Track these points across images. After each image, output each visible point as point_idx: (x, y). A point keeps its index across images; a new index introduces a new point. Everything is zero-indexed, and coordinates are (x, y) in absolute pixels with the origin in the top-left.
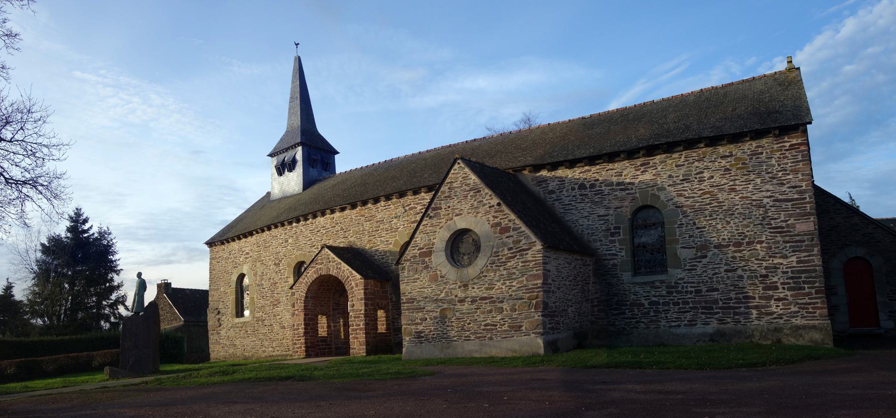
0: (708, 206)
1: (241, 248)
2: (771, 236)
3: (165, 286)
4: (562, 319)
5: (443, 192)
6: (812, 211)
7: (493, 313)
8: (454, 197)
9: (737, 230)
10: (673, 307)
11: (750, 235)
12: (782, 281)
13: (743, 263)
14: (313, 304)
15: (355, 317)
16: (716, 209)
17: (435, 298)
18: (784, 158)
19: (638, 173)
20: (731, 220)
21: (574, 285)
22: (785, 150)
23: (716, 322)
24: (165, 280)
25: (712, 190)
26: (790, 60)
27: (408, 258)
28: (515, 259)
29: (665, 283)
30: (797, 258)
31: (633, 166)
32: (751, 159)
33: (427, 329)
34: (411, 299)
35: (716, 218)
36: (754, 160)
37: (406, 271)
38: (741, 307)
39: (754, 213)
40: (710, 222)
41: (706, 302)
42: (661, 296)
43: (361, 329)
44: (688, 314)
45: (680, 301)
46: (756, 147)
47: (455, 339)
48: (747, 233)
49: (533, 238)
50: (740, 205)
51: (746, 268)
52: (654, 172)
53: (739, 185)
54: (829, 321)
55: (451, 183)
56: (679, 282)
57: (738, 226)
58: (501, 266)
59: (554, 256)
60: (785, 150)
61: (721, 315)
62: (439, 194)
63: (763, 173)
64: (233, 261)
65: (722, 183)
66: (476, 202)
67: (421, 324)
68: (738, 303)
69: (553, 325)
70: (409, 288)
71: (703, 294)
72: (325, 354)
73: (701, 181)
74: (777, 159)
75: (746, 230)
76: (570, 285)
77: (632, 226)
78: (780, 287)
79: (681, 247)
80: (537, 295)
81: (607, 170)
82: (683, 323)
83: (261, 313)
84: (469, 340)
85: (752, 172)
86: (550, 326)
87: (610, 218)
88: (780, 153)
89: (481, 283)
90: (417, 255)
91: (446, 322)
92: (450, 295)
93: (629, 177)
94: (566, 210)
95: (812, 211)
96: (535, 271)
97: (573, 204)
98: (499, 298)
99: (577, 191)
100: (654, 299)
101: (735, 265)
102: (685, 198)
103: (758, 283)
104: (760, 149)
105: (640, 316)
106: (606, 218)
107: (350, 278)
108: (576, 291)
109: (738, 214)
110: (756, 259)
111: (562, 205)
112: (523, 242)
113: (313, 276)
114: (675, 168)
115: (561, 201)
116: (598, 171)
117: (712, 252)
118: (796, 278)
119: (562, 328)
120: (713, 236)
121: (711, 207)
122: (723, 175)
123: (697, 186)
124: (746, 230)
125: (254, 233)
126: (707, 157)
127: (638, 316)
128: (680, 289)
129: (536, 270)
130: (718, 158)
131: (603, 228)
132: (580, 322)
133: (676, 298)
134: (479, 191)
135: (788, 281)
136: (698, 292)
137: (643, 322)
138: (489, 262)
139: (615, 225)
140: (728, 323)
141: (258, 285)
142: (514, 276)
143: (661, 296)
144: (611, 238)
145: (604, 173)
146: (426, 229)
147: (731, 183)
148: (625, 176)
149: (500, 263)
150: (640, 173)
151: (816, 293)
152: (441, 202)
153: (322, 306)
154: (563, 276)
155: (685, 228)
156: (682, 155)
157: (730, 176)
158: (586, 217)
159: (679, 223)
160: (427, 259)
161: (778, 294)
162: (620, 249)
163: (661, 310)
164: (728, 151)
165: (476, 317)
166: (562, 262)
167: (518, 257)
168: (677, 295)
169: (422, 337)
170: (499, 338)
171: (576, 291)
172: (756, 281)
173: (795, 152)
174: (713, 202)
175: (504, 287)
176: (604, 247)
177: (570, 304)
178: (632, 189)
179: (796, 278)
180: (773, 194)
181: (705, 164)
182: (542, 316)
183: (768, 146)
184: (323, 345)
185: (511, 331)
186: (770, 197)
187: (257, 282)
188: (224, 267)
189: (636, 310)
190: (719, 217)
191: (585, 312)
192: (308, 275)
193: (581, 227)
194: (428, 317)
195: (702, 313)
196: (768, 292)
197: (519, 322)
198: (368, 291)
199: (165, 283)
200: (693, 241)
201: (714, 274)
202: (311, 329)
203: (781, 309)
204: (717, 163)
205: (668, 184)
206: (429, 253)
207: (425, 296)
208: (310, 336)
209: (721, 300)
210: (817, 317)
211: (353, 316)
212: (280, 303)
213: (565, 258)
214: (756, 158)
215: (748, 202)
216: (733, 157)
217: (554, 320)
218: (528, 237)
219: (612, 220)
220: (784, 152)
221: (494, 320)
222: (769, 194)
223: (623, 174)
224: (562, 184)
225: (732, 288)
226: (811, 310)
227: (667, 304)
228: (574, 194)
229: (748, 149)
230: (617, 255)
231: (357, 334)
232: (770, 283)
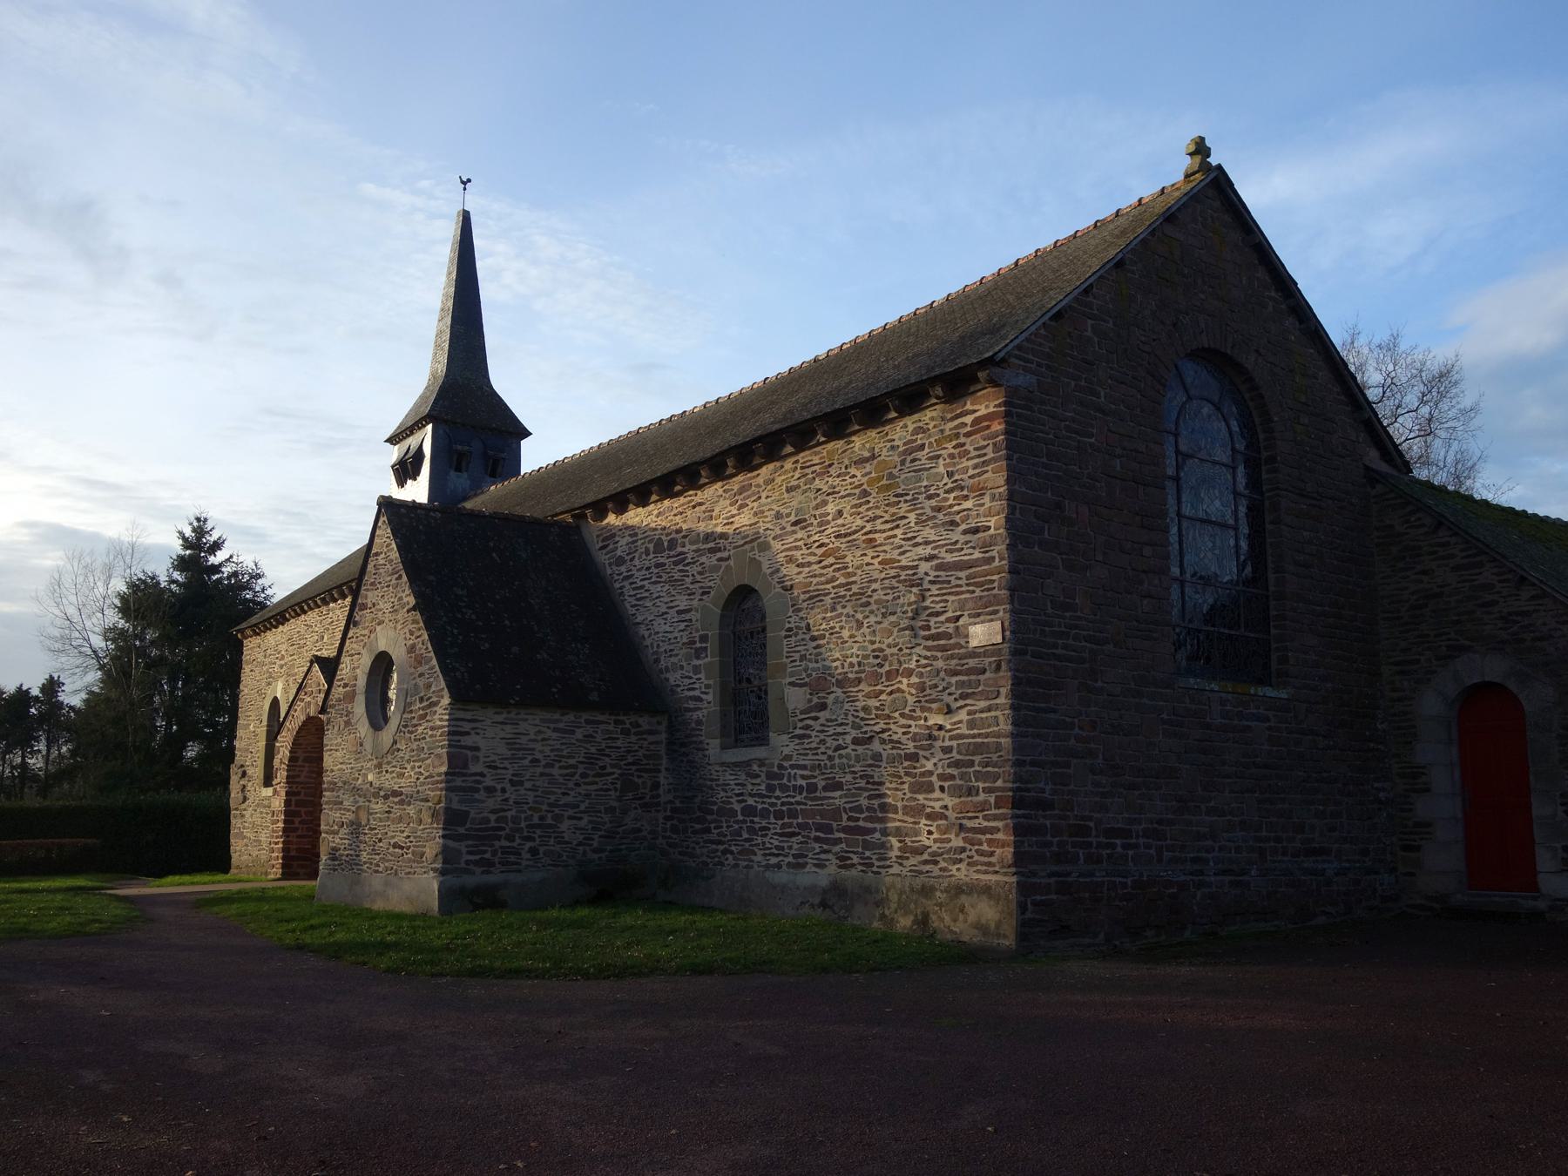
78: (937, 784)
88: (954, 443)
220: (962, 440)
222: (928, 550)
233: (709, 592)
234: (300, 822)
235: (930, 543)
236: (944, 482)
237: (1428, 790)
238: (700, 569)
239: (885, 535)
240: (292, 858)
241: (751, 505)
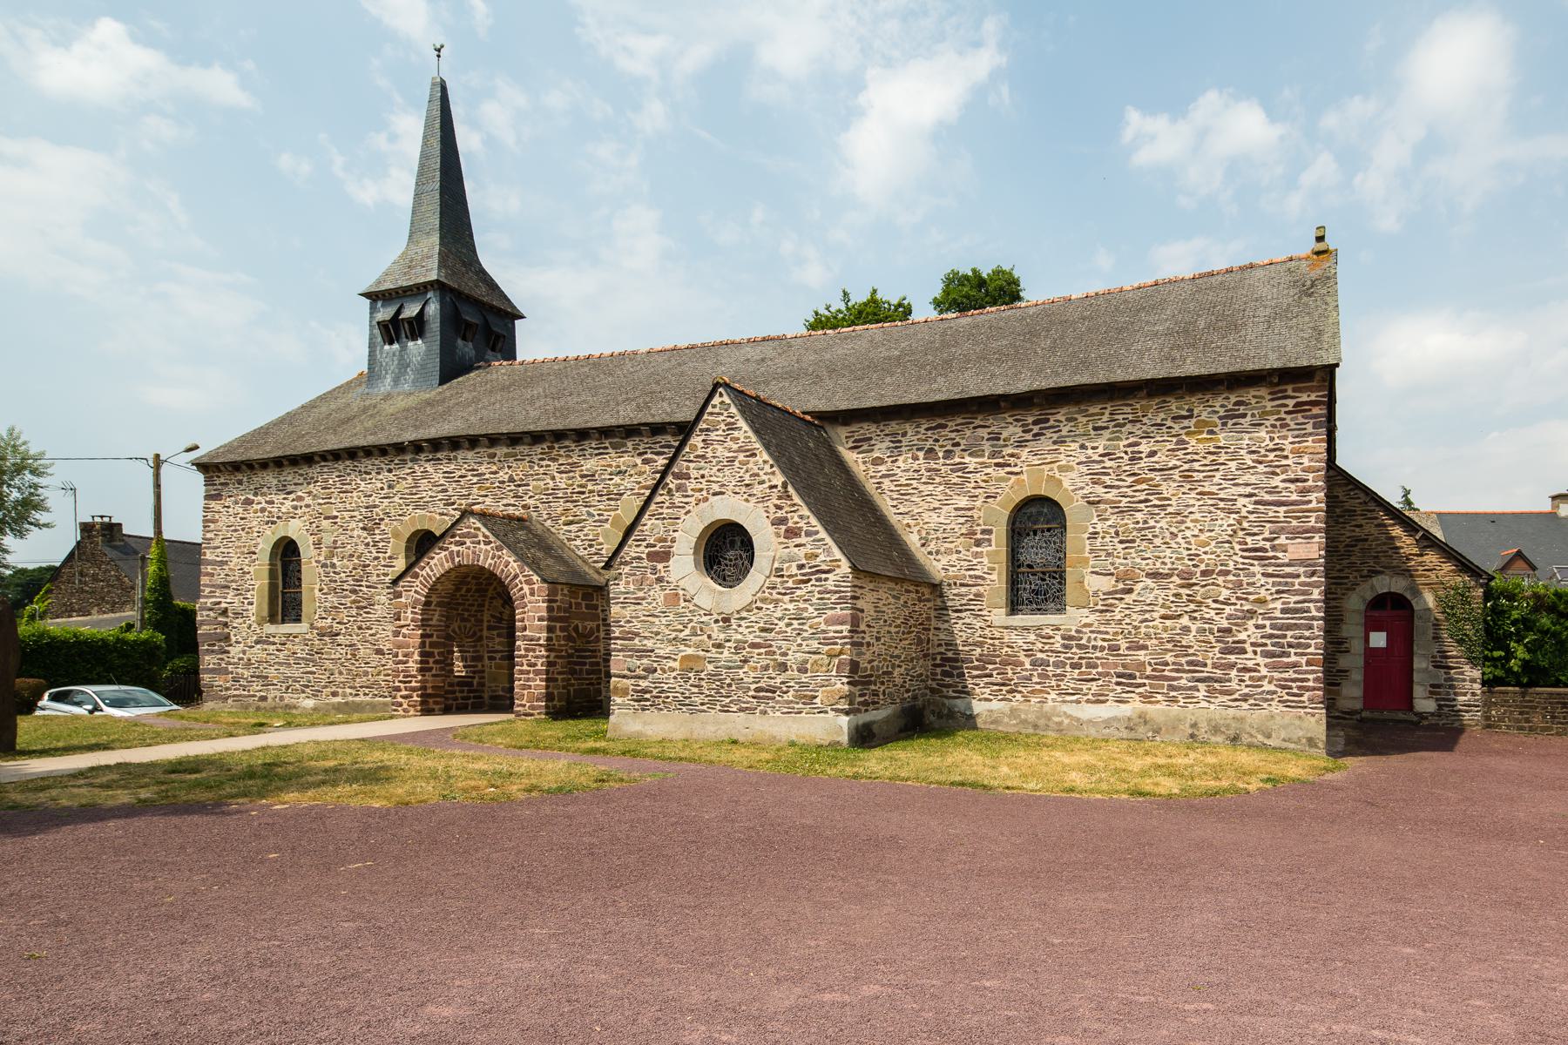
0: (1142, 505)
1: (285, 486)
2: (1243, 564)
3: (102, 529)
4: (883, 688)
5: (694, 448)
6: (1319, 525)
7: (770, 671)
8: (712, 459)
9: (1188, 549)
10: (1070, 670)
11: (1209, 559)
12: (1253, 640)
13: (1192, 606)
14: (443, 616)
15: (526, 650)
16: (1156, 511)
17: (674, 634)
18: (1282, 426)
19: (1029, 436)
20: (1180, 531)
21: (904, 633)
22: (1286, 412)
23: (1137, 698)
24: (102, 517)
25: (1152, 476)
26: (1321, 234)
27: (628, 559)
28: (809, 584)
29: (1059, 630)
30: (1283, 603)
31: (1020, 423)
32: (1224, 424)
33: (656, 688)
34: (629, 633)
35: (1154, 527)
36: (1229, 426)
37: (623, 582)
38: (1181, 678)
39: (1220, 522)
40: (1143, 533)
41: (1124, 666)
42: (1052, 651)
43: (537, 673)
44: (1094, 683)
45: (1083, 662)
46: (1235, 404)
47: (705, 707)
48: (1204, 556)
49: (838, 554)
50: (1196, 507)
51: (1195, 615)
52: (1055, 436)
53: (1198, 471)
54: (1324, 711)
55: (707, 430)
56: (1084, 630)
57: (1189, 543)
58: (785, 594)
59: (871, 586)
60: (1286, 412)
61: (1148, 688)
62: (687, 449)
63: (1243, 452)
64: (263, 510)
65: (1170, 465)
66: (748, 474)
67: (645, 678)
68: (1177, 671)
69: (867, 698)
70: (627, 613)
71: (1121, 652)
72: (467, 708)
73: (1134, 459)
74: (1270, 429)
75: (1203, 550)
76: (898, 632)
77: (1013, 531)
78: (1249, 649)
79: (1093, 572)
80: (842, 649)
81: (974, 428)
82: (1085, 698)
83: (329, 620)
84: (728, 711)
85: (1223, 448)
86: (862, 699)
87: (975, 514)
88: (1276, 417)
89: (753, 619)
90: (644, 556)
91: (690, 678)
92: (699, 633)
93: (1011, 442)
94: (902, 495)
95: (1319, 525)
96: (838, 610)
97: (914, 486)
98: (780, 648)
99: (921, 461)
100: (1040, 655)
101: (1179, 609)
102: (1106, 487)
103: (1213, 640)
104: (1242, 408)
105: (1016, 681)
106: (969, 513)
107: (521, 577)
108: (907, 642)
109: (1192, 521)
110: (1214, 601)
111: (896, 486)
112: (822, 557)
113: (442, 565)
114: (1092, 432)
115: (894, 478)
116: (958, 428)
117: (1141, 585)
118: (1278, 637)
119: (882, 702)
120: (1147, 556)
121: (1147, 507)
122: (1173, 450)
123: (1127, 468)
124: (1203, 550)
125: (317, 458)
126: (1150, 416)
127: (1012, 683)
128: (1083, 642)
129: (841, 609)
130: (1166, 420)
131: (964, 531)
132: (914, 690)
133: (1077, 657)
134: (754, 455)
135: (1264, 641)
136: (1114, 649)
137: (1020, 692)
138: (766, 585)
139: (983, 527)
140: (1158, 702)
141: (325, 565)
142: (805, 615)
143: (1052, 651)
144: (975, 549)
145: (968, 433)
146: (660, 511)
147: (1186, 467)
148: (1004, 440)
149: (784, 588)
150: (1030, 438)
151: (1309, 663)
152: (690, 464)
153: (463, 620)
154: (886, 618)
155: (1100, 540)
156: (1105, 408)
157: (1185, 454)
158: (935, 509)
159: (1091, 530)
160: (660, 566)
161: (1244, 661)
162: (989, 568)
163: (1050, 674)
164: (1186, 407)
165: (742, 676)
166: (879, 601)
167: (813, 582)
168: (1078, 651)
169: (647, 700)
170: (778, 714)
171: (907, 642)
172: (1211, 637)
173: (1303, 417)
174: (1151, 498)
175: (789, 629)
176: (962, 563)
177: (897, 663)
178: (1016, 465)
179: (1278, 637)
180: (1256, 491)
181: (1144, 428)
182: (848, 683)
183: (1257, 403)
184: (462, 692)
185: (798, 703)
186: (1251, 495)
187: (322, 558)
188: (242, 519)
189: (1010, 672)
190: (1159, 525)
191: (921, 675)
192: (432, 562)
193: (925, 527)
194: (658, 668)
195: (1118, 684)
196: (1228, 656)
197: (811, 691)
198: (555, 605)
199: (102, 524)
200: (1113, 564)
201: (1142, 622)
202: (434, 662)
203: (1247, 686)
204: (1164, 428)
205: (1078, 461)
206: (664, 556)
207: (655, 630)
208: (433, 676)
209: (1150, 664)
210: (1304, 702)
211: (523, 647)
212: (373, 605)
213: (889, 589)
214: (1234, 424)
215: (1210, 502)
216: (1194, 420)
217: (868, 689)
218: (828, 551)
219: (979, 518)
220: (1284, 416)
221: (772, 682)
222: (1248, 490)
223: (1002, 437)
224: (896, 448)
225: (1169, 646)
226: (1295, 691)
227: (1062, 664)
228: (915, 467)
229: (1222, 406)
230: (984, 579)
231: (528, 680)
232: (1234, 642)
233: (996, 497)
234: (434, 662)
235: (1250, 485)
236: (1265, 443)
237: (1348, 652)
238: (985, 478)
239: (1205, 474)
240: (430, 696)
241: (1048, 435)
